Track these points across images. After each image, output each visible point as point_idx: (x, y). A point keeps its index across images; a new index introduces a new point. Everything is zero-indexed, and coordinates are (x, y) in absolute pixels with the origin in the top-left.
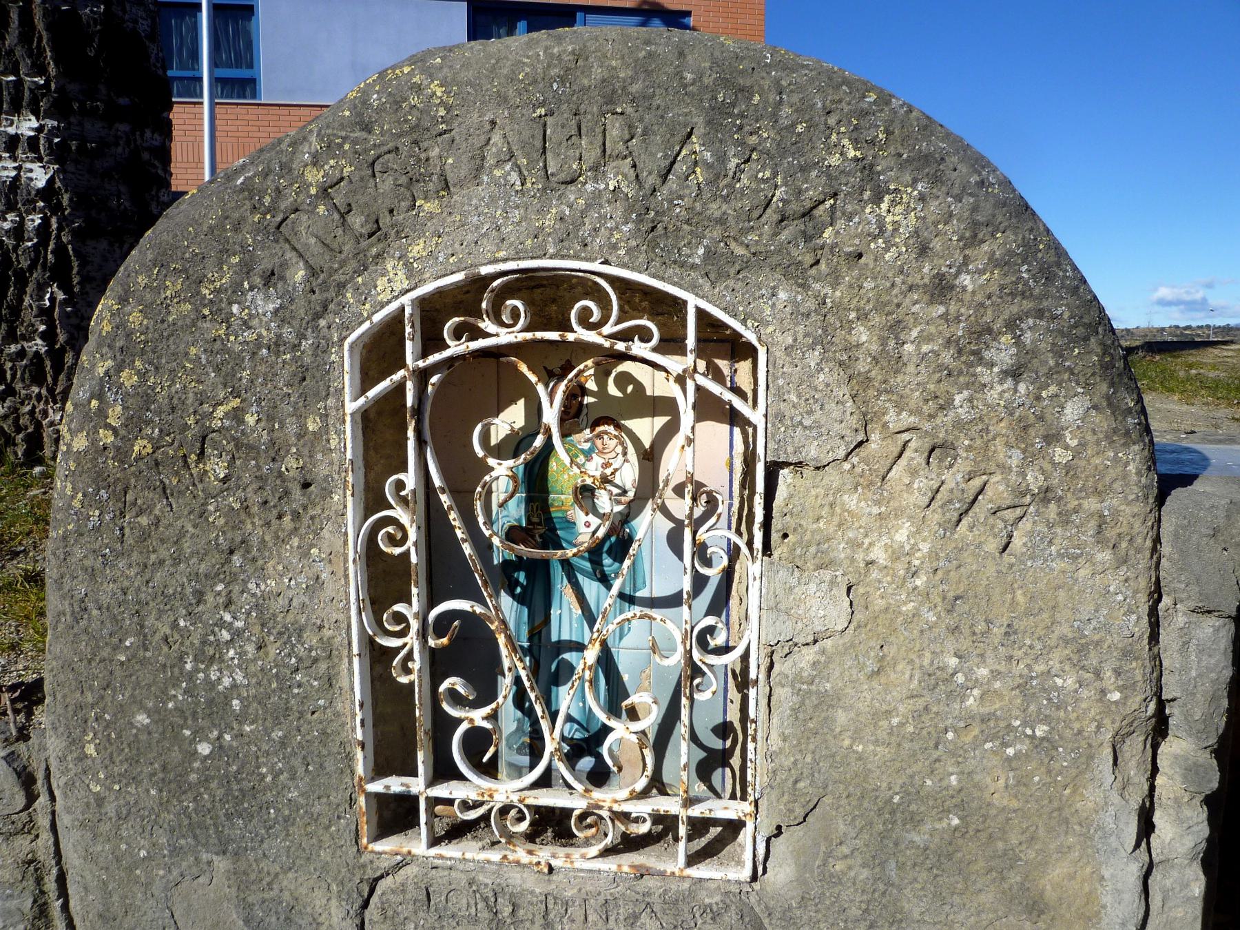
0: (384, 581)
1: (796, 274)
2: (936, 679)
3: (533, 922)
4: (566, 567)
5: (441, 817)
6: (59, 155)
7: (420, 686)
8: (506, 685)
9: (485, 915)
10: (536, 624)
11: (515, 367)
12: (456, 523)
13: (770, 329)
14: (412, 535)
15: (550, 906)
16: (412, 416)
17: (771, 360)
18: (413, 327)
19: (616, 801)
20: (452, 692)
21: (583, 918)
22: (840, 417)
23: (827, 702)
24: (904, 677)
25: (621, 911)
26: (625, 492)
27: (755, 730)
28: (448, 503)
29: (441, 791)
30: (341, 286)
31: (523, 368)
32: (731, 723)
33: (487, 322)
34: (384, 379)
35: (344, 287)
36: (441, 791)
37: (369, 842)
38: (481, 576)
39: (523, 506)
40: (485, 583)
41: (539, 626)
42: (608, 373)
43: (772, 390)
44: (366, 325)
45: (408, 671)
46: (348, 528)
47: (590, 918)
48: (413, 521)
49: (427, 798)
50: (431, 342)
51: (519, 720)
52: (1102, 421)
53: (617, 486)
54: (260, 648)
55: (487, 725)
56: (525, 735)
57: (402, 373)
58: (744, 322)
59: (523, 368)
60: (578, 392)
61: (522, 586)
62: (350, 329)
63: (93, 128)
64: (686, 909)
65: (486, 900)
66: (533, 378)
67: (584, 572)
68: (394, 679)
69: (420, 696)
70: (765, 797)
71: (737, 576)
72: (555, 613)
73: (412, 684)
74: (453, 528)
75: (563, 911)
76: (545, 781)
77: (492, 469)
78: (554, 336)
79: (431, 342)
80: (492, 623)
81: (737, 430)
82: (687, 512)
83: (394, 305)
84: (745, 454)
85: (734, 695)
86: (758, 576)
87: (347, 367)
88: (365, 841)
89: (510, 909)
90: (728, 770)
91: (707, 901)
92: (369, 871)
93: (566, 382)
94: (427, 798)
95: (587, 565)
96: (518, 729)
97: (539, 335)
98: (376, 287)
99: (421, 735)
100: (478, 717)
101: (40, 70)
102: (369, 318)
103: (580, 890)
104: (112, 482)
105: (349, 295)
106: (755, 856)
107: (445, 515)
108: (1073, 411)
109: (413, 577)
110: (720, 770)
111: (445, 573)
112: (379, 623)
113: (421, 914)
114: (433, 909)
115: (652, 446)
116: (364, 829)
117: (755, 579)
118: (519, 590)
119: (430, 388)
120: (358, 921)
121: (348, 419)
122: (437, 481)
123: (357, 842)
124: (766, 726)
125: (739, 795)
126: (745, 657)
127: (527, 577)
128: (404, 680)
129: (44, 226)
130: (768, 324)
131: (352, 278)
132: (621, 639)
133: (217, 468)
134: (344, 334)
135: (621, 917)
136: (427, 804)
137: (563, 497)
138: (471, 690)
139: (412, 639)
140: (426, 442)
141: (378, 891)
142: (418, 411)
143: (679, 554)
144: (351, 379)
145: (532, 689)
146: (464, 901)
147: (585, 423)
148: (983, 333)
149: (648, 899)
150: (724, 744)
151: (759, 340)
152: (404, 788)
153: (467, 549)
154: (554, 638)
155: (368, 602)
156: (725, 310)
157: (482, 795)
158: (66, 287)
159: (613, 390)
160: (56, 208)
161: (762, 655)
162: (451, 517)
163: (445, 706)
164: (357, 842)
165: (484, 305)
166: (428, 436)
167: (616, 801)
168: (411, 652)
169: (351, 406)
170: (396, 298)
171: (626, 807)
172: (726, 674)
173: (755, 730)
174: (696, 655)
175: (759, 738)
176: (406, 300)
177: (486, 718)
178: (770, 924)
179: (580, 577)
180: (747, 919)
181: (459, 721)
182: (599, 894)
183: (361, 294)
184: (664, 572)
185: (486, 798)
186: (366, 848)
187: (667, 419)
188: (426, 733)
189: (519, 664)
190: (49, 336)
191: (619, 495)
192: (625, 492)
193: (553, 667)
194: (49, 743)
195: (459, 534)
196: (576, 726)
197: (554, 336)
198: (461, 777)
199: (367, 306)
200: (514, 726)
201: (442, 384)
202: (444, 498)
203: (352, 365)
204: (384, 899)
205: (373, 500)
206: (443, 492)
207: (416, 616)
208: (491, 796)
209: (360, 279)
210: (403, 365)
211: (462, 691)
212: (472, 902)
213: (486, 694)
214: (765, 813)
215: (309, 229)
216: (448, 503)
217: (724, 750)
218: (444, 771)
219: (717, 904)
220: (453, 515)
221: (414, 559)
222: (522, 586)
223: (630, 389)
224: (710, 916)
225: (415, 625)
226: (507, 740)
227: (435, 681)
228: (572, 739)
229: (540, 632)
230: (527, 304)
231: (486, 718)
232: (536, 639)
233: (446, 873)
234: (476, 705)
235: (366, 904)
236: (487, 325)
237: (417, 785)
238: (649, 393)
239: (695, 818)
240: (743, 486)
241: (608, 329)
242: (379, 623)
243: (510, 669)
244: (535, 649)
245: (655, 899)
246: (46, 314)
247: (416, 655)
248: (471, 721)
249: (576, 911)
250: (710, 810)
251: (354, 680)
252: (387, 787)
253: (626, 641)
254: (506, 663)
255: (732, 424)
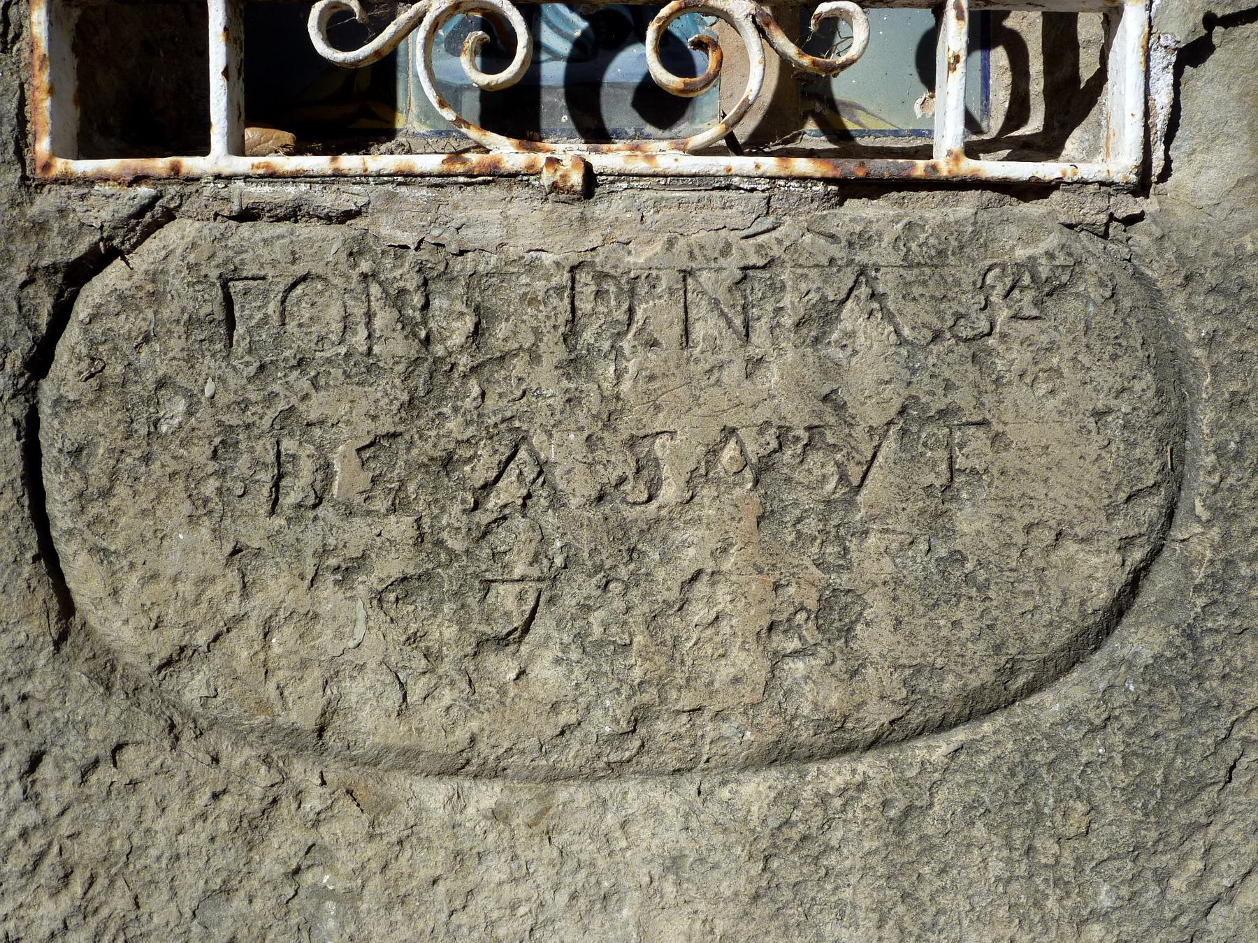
3: (534, 357)
9: (396, 347)
15: (584, 306)
21: (678, 329)
25: (788, 300)
37: (55, 153)
47: (699, 331)
54: (589, 608)
64: (968, 276)
65: (397, 299)
75: (621, 316)
88: (43, 146)
89: (469, 323)
91: (1021, 254)
92: (55, 241)
103: (671, 243)
106: (1147, 114)
113: (207, 364)
114: (240, 347)
116: (42, 108)
120: (19, 410)
123: (19, 153)
125: (919, 142)
135: (788, 321)
141: (81, 310)
146: (335, 312)
149: (861, 257)
164: (19, 153)
178: (1191, 308)
180: (1127, 303)
182: (726, 251)
186: (47, 167)
204: (97, 329)
212: (358, 311)
219: (1050, 255)
224: (1029, 295)
233: (283, 228)
235: (39, 361)
239: (971, 33)
245: (881, 254)
249: (657, 312)
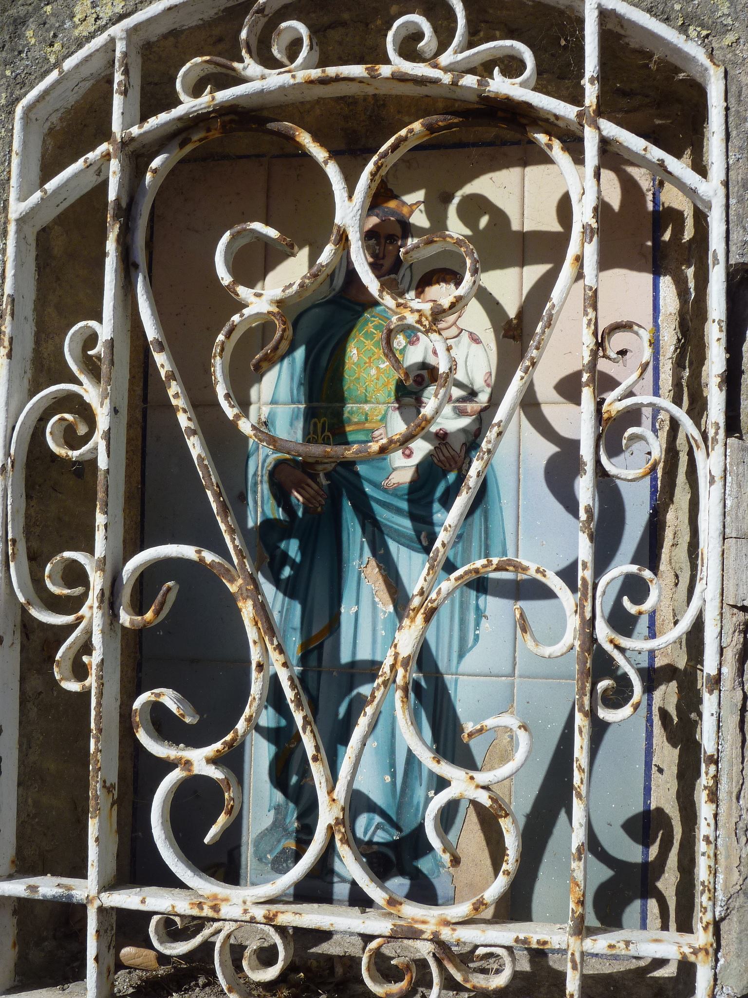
4: (369, 528)
5: (131, 968)
7: (100, 694)
8: (255, 709)
10: (315, 632)
11: (290, 139)
12: (179, 402)
13: (730, 38)
14: (103, 421)
16: (116, 217)
17: (733, 89)
18: (126, 72)
19: (447, 923)
20: (157, 709)
26: (472, 394)
27: (716, 778)
28: (168, 367)
29: (128, 899)
30: (20, 22)
31: (305, 139)
32: (659, 810)
33: (248, 59)
34: (75, 160)
35: (24, 23)
36: (128, 899)
38: (218, 495)
39: (300, 424)
40: (224, 507)
41: (321, 634)
42: (447, 198)
43: (735, 142)
44: (54, 75)
45: (80, 671)
48: (104, 396)
49: (101, 910)
50: (155, 96)
51: (278, 808)
53: (459, 385)
55: (215, 773)
56: (287, 834)
57: (104, 147)
58: (683, 29)
59: (305, 139)
60: (398, 231)
61: (293, 564)
62: (24, 83)
66: (319, 153)
67: (400, 538)
68: (56, 683)
69: (100, 716)
70: (734, 917)
71: (669, 534)
72: (347, 610)
73: (85, 695)
74: (173, 410)
76: (316, 888)
77: (242, 305)
79: (155, 96)
80: (232, 580)
81: (667, 283)
82: (587, 359)
83: (99, 41)
84: (682, 315)
85: (667, 755)
86: (717, 473)
87: (16, 145)
90: (653, 905)
93: (375, 158)
94: (101, 910)
95: (405, 524)
96: (275, 825)
97: (332, 71)
98: (72, 17)
99: (96, 787)
100: (200, 760)
102: (58, 64)
105: (29, 33)
107: (163, 388)
109: (100, 495)
110: (637, 904)
111: (158, 498)
112: (37, 581)
115: (520, 315)
117: (712, 481)
118: (287, 572)
119: (149, 176)
121: (12, 228)
122: (151, 332)
124: (737, 768)
126: (694, 639)
127: (302, 549)
128: (73, 686)
130: (726, 30)
131: (38, 9)
132: (461, 656)
134: (17, 92)
136: (100, 922)
137: (367, 407)
138: (190, 709)
139: (92, 612)
140: (136, 266)
142: (126, 214)
143: (571, 505)
144: (22, 165)
145: (299, 704)
147: (407, 279)
150: (646, 854)
151: (711, 55)
152: (60, 891)
153: (195, 447)
154: (345, 657)
155: (22, 546)
156: (649, 11)
157: (200, 906)
159: (456, 228)
161: (729, 627)
162: (171, 392)
163: (143, 737)
165: (244, 34)
166: (140, 255)
167: (447, 923)
168: (89, 633)
169: (16, 209)
170: (103, 29)
171: (470, 935)
172: (649, 720)
173: (716, 778)
174: (603, 631)
175: (722, 795)
176: (117, 30)
177: (213, 761)
179: (393, 546)
181: (167, 766)
183: (48, 31)
184: (543, 536)
185: (207, 912)
187: (548, 267)
188: (107, 788)
189: (274, 656)
191: (462, 400)
192: (472, 394)
193: (342, 710)
195: (183, 420)
196: (378, 819)
198: (171, 881)
199: (57, 46)
200: (268, 819)
201: (173, 175)
202: (161, 359)
203: (25, 143)
205: (44, 366)
206: (161, 349)
207: (102, 565)
208: (215, 908)
209: (49, 8)
210: (106, 134)
211: (173, 706)
213: (217, 708)
214: (733, 948)
216: (168, 367)
217: (645, 865)
218: (137, 865)
220: (174, 388)
221: (103, 463)
222: (293, 564)
223: (484, 221)
225: (97, 581)
226: (257, 844)
227: (133, 686)
228: (370, 843)
229: (320, 647)
230: (314, 31)
231: (213, 761)
232: (313, 661)
234: (195, 737)
236: (250, 67)
237: (84, 889)
238: (515, 226)
240: (679, 364)
241: (445, 59)
242: (37, 581)
243: (260, 666)
244: (311, 677)
247: (97, 640)
248: (188, 764)
250: (627, 943)
252: (33, 888)
253: (470, 662)
254: (255, 655)
255: (657, 273)
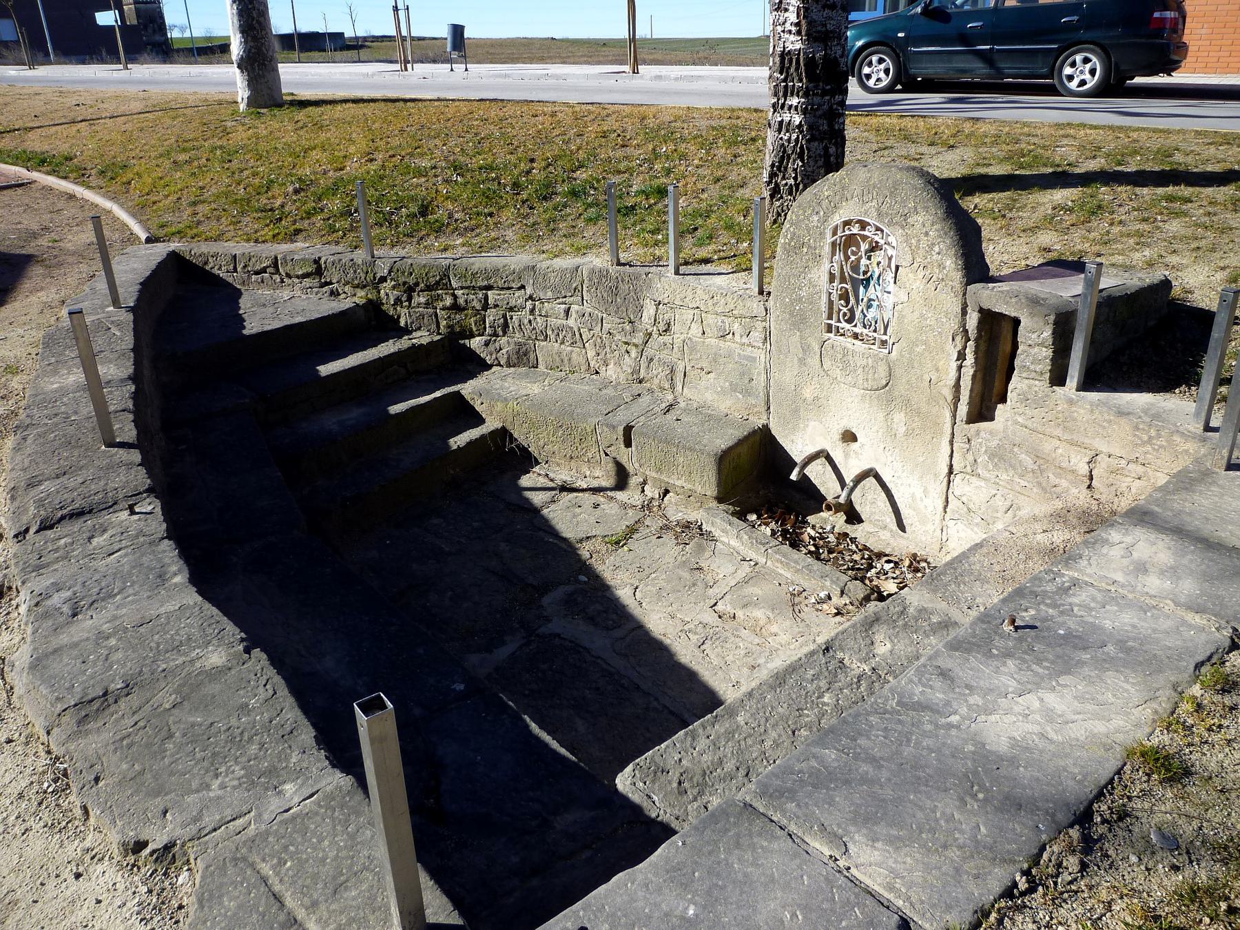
0: (832, 277)
1: (903, 227)
2: (922, 316)
6: (805, 112)
22: (909, 258)
23: (904, 317)
24: (916, 314)
46: (826, 266)
52: (953, 266)
63: (817, 100)
78: (387, 348)
101: (801, 80)
104: (787, 251)
108: (948, 263)
129: (797, 140)
133: (805, 250)
148: (933, 244)
158: (802, 161)
160: (801, 132)
190: (795, 178)
194: (771, 303)
197: (387, 348)
215: (825, 203)
246: (795, 170)
251: (824, 299)
